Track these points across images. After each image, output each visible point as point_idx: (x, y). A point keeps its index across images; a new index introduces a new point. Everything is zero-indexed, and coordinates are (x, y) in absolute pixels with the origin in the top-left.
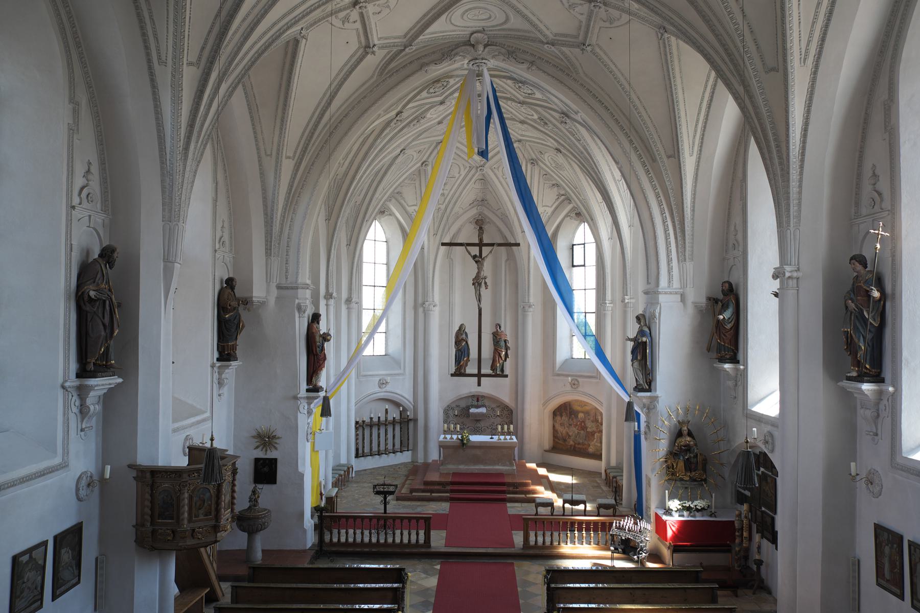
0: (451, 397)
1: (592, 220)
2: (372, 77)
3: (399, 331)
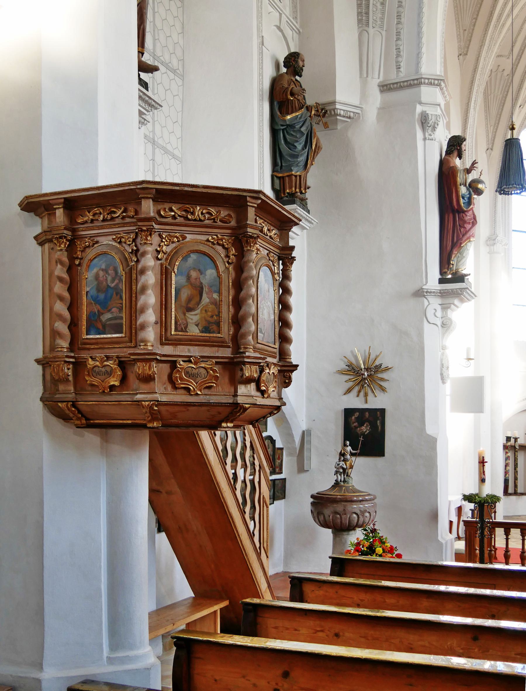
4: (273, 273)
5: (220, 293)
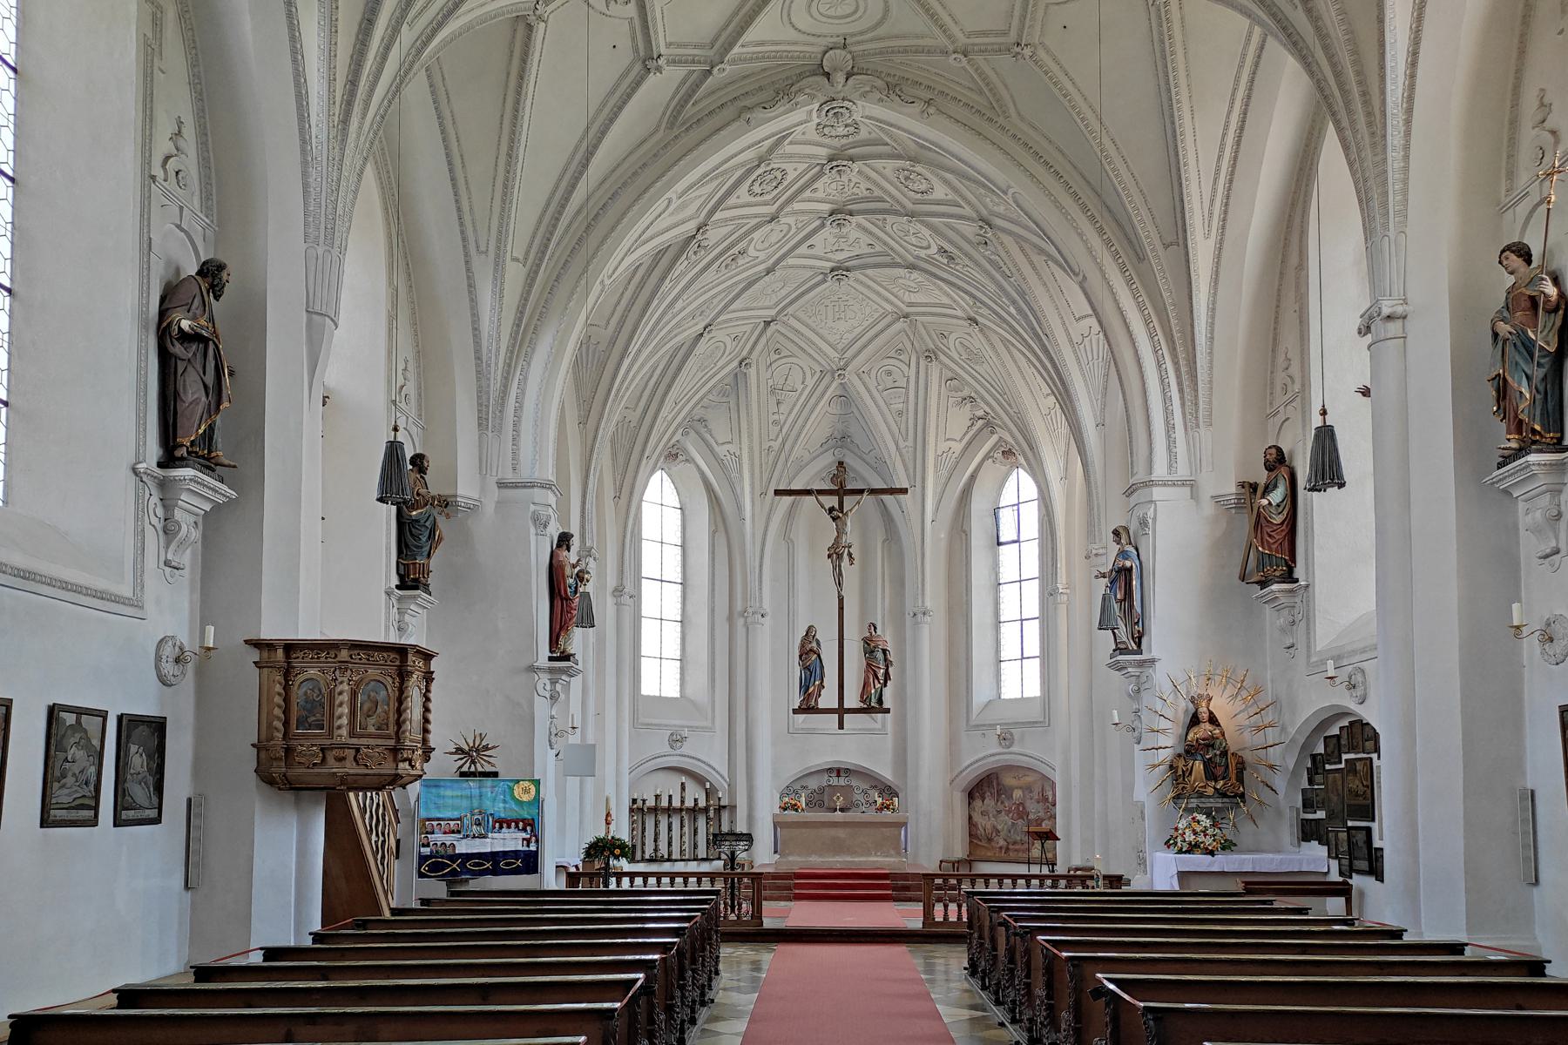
0: (792, 770)
1: (1032, 448)
2: (656, 130)
3: (704, 657)
4: (420, 689)
5: (388, 705)
